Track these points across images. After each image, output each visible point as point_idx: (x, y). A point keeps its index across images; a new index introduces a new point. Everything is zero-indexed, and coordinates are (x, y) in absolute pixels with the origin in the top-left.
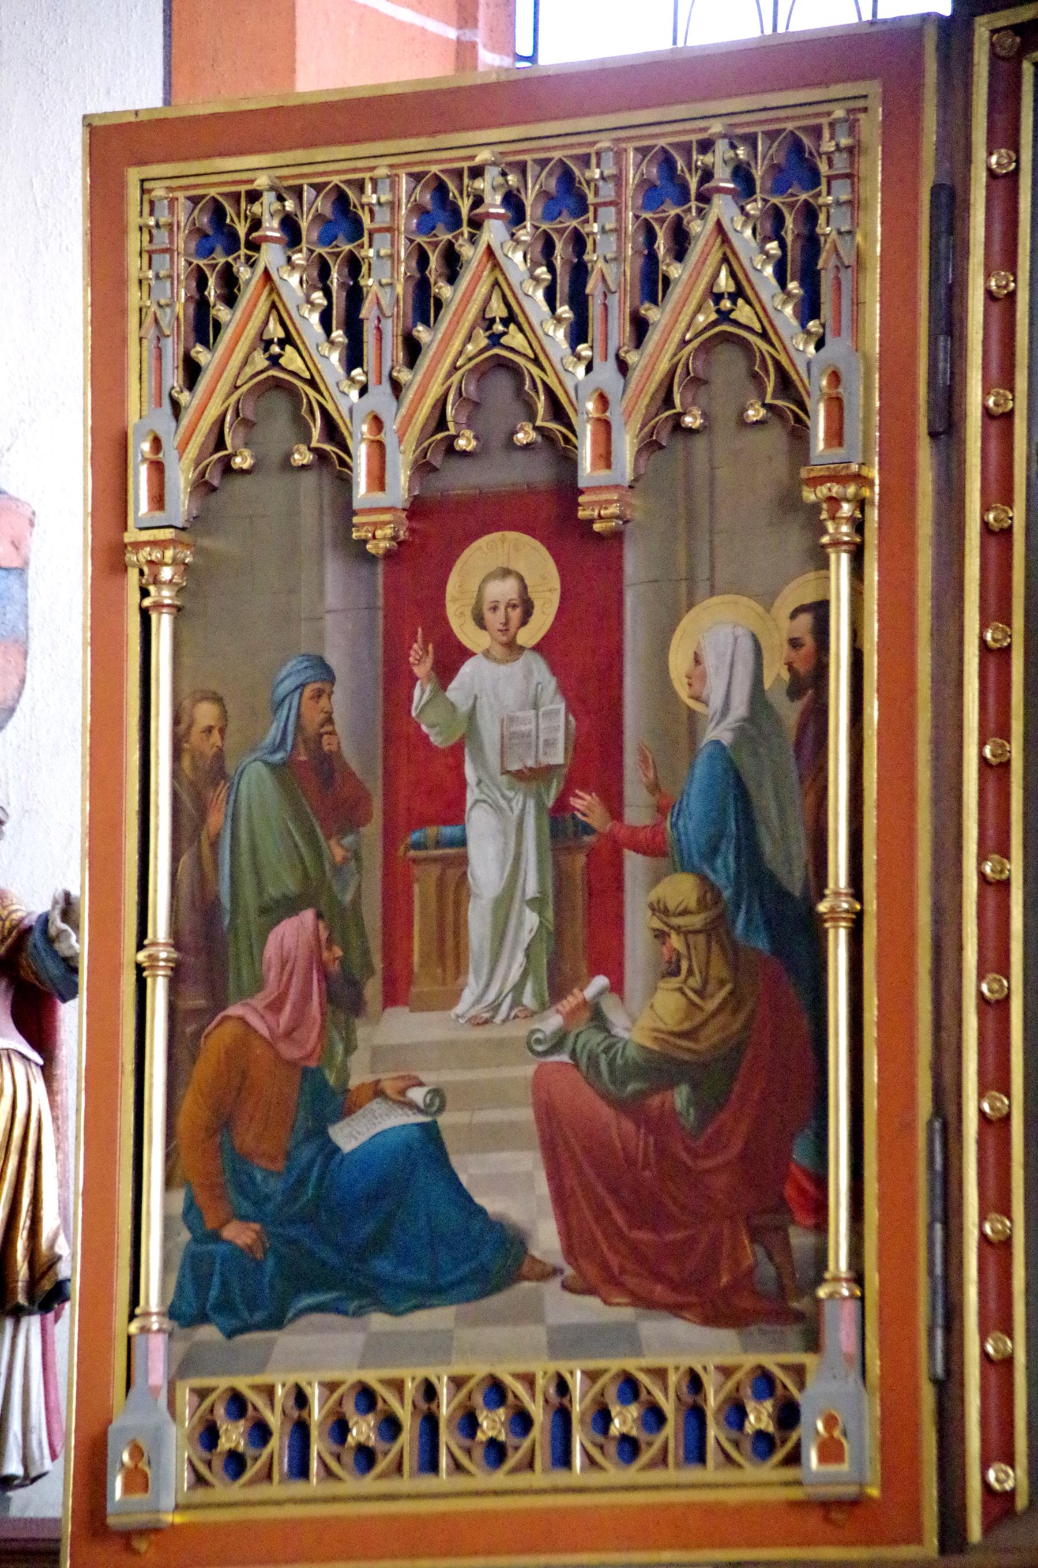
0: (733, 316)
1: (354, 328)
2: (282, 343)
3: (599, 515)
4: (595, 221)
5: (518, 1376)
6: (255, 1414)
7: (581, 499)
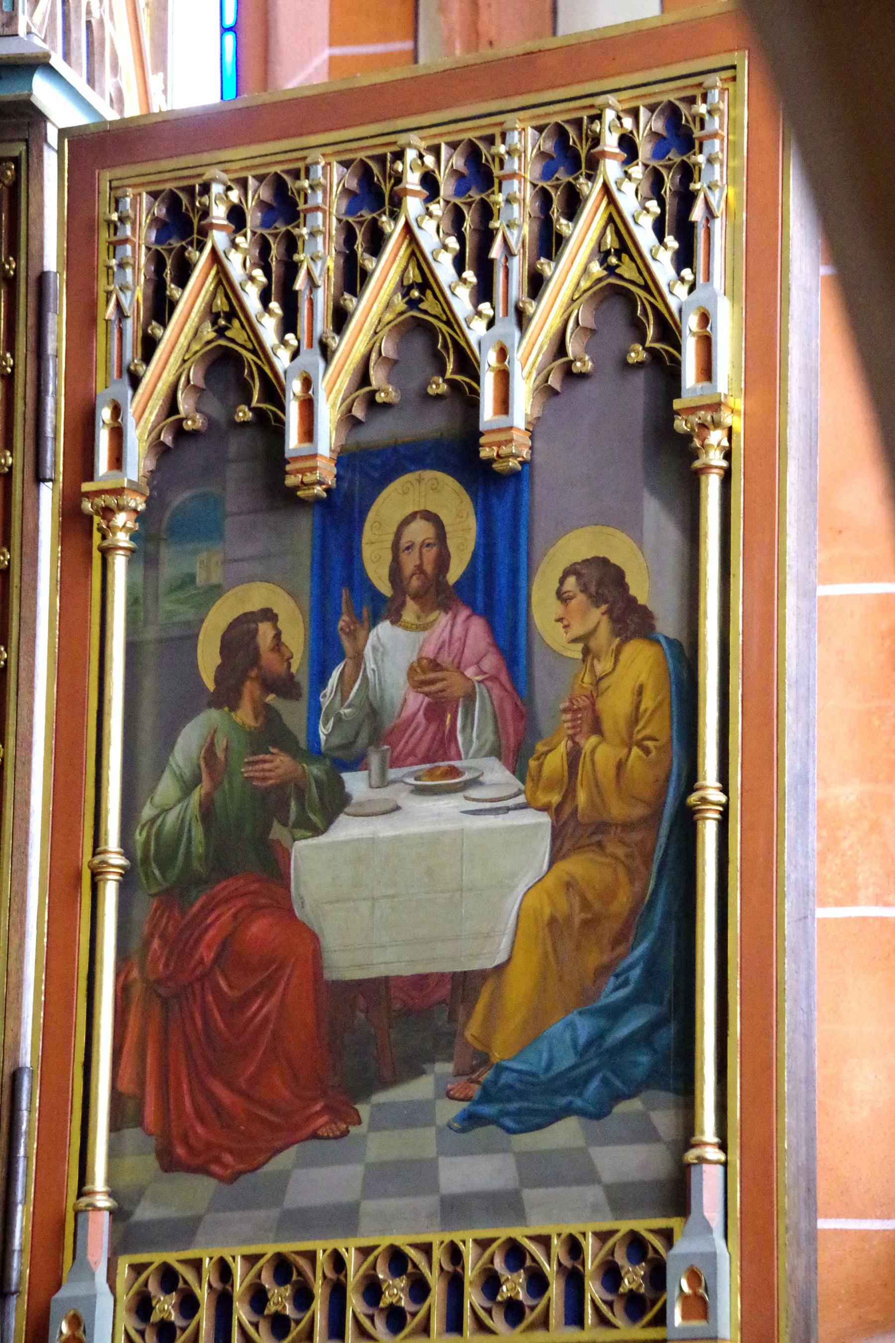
0: (618, 271)
1: (485, 269)
2: (618, 253)
3: (498, 455)
4: (305, 225)
5: (415, 1246)
6: (655, 1256)
7: (482, 440)
